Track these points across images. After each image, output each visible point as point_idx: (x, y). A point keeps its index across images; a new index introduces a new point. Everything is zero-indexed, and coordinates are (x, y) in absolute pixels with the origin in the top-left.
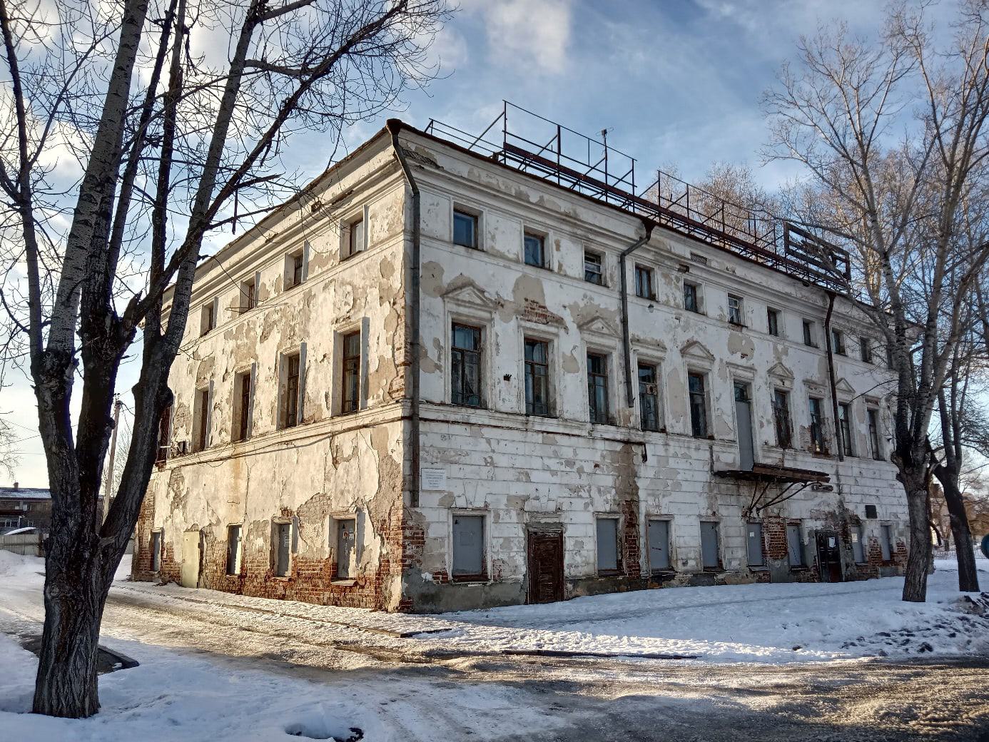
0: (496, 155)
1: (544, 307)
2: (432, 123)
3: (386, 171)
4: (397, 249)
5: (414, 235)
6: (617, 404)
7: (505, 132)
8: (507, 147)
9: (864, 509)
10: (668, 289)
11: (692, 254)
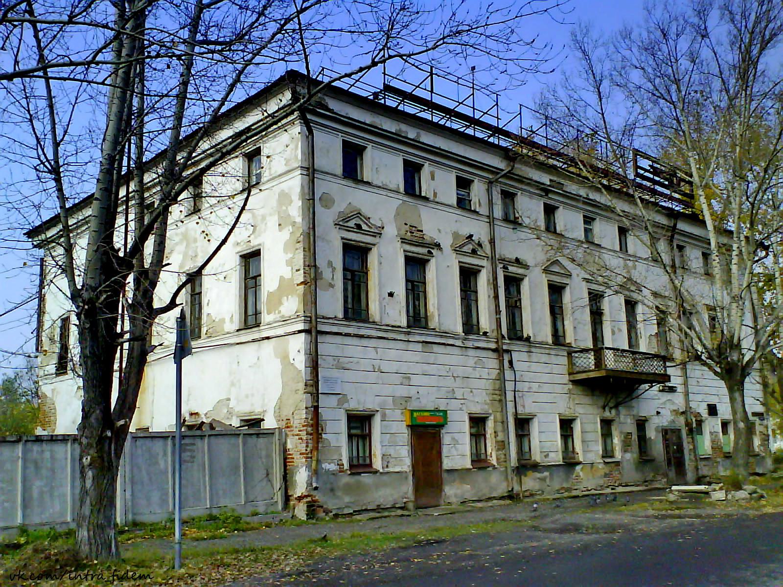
0: (376, 95)
1: (422, 231)
2: (323, 70)
3: (285, 111)
4: (295, 183)
5: (311, 172)
6: (485, 321)
7: (384, 73)
8: (388, 88)
9: (706, 407)
10: (530, 208)
11: (551, 180)
